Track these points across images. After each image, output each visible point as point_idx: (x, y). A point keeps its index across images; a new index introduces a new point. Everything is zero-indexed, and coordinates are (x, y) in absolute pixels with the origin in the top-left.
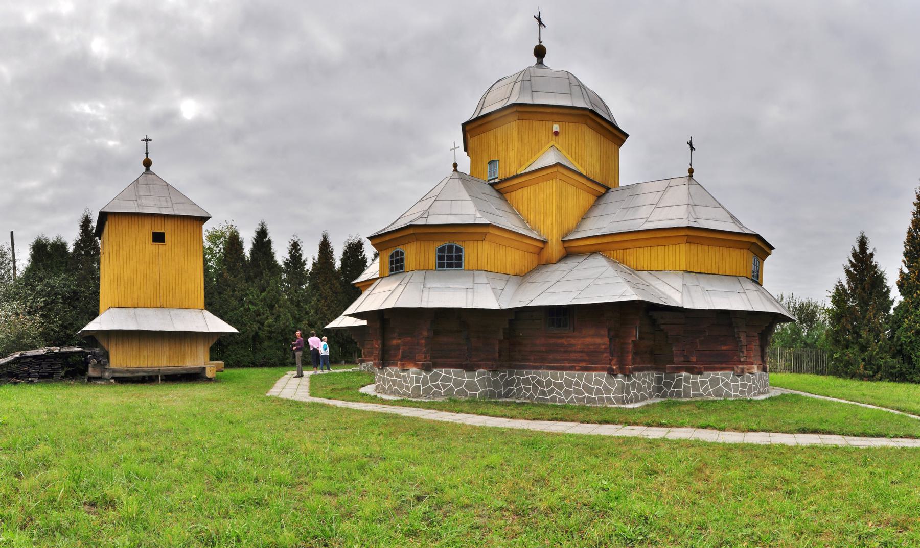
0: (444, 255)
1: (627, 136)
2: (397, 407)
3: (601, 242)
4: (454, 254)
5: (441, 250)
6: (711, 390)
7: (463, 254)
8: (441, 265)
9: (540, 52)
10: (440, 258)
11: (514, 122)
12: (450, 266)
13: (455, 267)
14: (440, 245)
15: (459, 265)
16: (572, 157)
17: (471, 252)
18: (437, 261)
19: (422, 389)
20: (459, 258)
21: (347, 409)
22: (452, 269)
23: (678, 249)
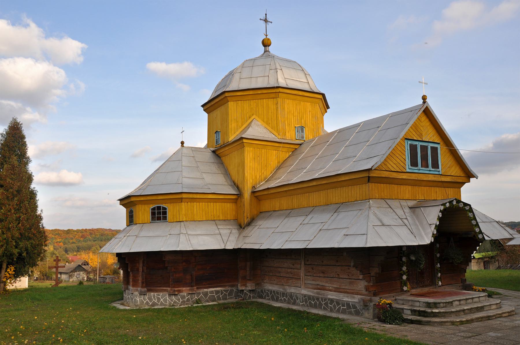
0: (157, 215)
1: (330, 108)
2: (478, 313)
3: (240, 95)
4: (162, 211)
5: (153, 209)
6: (162, 300)
7: (167, 210)
8: (153, 219)
9: (266, 44)
10: (153, 214)
11: (237, 151)
12: (159, 219)
13: (163, 220)
14: (152, 206)
15: (165, 218)
16: (264, 122)
17: (171, 210)
18: (162, 221)
19: (340, 305)
20: (165, 213)
21: (178, 288)
22: (161, 221)
23: (336, 215)
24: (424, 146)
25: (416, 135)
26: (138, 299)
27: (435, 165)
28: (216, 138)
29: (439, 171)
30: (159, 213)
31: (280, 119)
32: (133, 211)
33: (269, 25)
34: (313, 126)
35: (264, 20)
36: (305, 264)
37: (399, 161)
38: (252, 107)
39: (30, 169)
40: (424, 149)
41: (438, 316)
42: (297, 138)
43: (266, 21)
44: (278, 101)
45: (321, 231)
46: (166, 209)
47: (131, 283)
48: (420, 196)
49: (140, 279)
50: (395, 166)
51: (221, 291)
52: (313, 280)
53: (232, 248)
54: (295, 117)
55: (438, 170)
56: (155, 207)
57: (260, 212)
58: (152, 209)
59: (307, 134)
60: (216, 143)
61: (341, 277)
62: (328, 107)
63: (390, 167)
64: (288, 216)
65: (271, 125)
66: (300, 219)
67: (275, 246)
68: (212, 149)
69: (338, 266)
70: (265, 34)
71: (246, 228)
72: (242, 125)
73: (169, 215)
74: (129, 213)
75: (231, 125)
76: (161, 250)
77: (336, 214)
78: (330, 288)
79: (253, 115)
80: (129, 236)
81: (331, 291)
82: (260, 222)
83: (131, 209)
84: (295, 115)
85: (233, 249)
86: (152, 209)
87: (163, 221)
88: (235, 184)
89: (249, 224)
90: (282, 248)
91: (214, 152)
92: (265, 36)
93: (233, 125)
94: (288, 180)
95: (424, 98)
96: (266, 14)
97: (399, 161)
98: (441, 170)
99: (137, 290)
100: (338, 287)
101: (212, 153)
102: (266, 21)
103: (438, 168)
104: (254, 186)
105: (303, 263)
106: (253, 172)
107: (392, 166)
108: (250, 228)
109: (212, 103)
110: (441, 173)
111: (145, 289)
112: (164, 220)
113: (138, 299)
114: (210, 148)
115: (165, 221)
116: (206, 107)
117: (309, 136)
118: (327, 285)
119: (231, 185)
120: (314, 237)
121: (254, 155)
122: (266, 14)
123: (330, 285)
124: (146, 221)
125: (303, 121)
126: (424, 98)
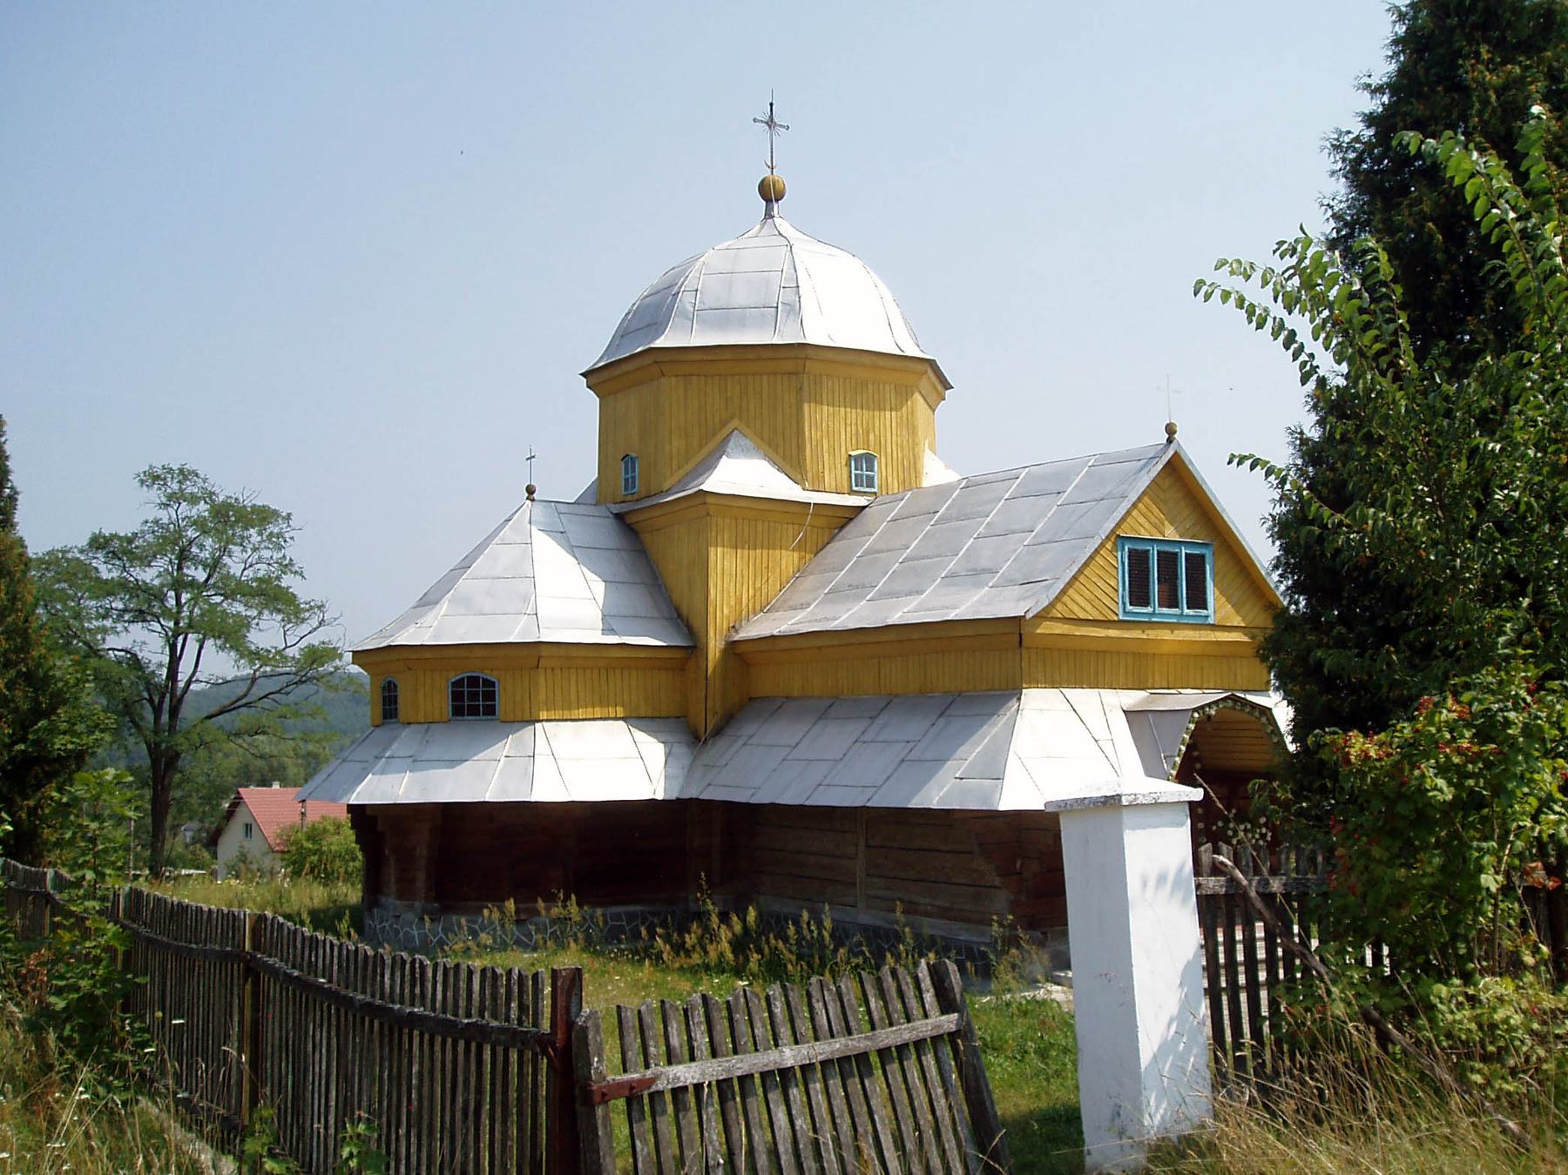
8: (458, 711)
10: (457, 696)
12: (474, 711)
15: (491, 711)
16: (762, 439)
18: (482, 717)
20: (490, 696)
24: (1167, 553)
25: (1147, 525)
26: (416, 933)
27: (1198, 600)
28: (626, 473)
29: (1207, 617)
30: (474, 696)
31: (807, 434)
32: (395, 686)
33: (781, 137)
34: (902, 451)
35: (767, 123)
36: (867, 846)
37: (1099, 593)
38: (729, 394)
39: (16, 516)
40: (1168, 560)
41: (210, 752)
42: (855, 488)
43: (770, 123)
44: (802, 384)
45: (904, 765)
46: (492, 684)
47: (393, 888)
48: (1157, 678)
49: (421, 877)
50: (1089, 607)
51: (643, 912)
52: (888, 888)
53: (674, 798)
54: (848, 429)
55: (1204, 612)
56: (463, 679)
57: (750, 699)
58: (453, 683)
59: (884, 474)
60: (626, 489)
61: (954, 880)
62: (947, 386)
63: (1076, 609)
64: (823, 715)
65: (781, 450)
66: (854, 729)
67: (789, 798)
68: (616, 509)
69: (948, 852)
70: (770, 164)
71: (710, 742)
72: (701, 446)
73: (501, 702)
74: (380, 690)
75: (671, 443)
76: (487, 800)
77: (942, 721)
78: (929, 908)
79: (732, 418)
80: (393, 757)
81: (929, 915)
82: (749, 728)
83: (389, 679)
84: (849, 422)
85: (678, 799)
86: (455, 684)
87: (484, 717)
88: (680, 616)
89: (718, 732)
90: (806, 803)
91: (619, 517)
92: (769, 170)
93: (675, 444)
94: (827, 619)
95: (1170, 430)
96: (771, 105)
97: (1099, 593)
98: (1212, 615)
99: (411, 907)
100: (947, 905)
101: (613, 520)
102: (770, 123)
103: (1205, 608)
104: (733, 627)
105: (862, 843)
106: (733, 584)
107: (1079, 605)
108: (722, 743)
109: (615, 372)
110: (1211, 621)
111: (436, 905)
112: (488, 715)
113: (416, 933)
114: (608, 505)
115: (489, 717)
116: (595, 380)
117: (890, 480)
118: (921, 900)
119: (670, 619)
120: (885, 778)
121: (734, 539)
122: (771, 105)
123: (928, 901)
124: (437, 717)
125: (872, 437)
126: (1170, 430)
